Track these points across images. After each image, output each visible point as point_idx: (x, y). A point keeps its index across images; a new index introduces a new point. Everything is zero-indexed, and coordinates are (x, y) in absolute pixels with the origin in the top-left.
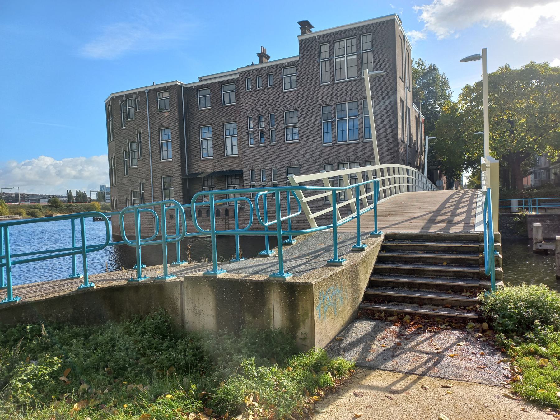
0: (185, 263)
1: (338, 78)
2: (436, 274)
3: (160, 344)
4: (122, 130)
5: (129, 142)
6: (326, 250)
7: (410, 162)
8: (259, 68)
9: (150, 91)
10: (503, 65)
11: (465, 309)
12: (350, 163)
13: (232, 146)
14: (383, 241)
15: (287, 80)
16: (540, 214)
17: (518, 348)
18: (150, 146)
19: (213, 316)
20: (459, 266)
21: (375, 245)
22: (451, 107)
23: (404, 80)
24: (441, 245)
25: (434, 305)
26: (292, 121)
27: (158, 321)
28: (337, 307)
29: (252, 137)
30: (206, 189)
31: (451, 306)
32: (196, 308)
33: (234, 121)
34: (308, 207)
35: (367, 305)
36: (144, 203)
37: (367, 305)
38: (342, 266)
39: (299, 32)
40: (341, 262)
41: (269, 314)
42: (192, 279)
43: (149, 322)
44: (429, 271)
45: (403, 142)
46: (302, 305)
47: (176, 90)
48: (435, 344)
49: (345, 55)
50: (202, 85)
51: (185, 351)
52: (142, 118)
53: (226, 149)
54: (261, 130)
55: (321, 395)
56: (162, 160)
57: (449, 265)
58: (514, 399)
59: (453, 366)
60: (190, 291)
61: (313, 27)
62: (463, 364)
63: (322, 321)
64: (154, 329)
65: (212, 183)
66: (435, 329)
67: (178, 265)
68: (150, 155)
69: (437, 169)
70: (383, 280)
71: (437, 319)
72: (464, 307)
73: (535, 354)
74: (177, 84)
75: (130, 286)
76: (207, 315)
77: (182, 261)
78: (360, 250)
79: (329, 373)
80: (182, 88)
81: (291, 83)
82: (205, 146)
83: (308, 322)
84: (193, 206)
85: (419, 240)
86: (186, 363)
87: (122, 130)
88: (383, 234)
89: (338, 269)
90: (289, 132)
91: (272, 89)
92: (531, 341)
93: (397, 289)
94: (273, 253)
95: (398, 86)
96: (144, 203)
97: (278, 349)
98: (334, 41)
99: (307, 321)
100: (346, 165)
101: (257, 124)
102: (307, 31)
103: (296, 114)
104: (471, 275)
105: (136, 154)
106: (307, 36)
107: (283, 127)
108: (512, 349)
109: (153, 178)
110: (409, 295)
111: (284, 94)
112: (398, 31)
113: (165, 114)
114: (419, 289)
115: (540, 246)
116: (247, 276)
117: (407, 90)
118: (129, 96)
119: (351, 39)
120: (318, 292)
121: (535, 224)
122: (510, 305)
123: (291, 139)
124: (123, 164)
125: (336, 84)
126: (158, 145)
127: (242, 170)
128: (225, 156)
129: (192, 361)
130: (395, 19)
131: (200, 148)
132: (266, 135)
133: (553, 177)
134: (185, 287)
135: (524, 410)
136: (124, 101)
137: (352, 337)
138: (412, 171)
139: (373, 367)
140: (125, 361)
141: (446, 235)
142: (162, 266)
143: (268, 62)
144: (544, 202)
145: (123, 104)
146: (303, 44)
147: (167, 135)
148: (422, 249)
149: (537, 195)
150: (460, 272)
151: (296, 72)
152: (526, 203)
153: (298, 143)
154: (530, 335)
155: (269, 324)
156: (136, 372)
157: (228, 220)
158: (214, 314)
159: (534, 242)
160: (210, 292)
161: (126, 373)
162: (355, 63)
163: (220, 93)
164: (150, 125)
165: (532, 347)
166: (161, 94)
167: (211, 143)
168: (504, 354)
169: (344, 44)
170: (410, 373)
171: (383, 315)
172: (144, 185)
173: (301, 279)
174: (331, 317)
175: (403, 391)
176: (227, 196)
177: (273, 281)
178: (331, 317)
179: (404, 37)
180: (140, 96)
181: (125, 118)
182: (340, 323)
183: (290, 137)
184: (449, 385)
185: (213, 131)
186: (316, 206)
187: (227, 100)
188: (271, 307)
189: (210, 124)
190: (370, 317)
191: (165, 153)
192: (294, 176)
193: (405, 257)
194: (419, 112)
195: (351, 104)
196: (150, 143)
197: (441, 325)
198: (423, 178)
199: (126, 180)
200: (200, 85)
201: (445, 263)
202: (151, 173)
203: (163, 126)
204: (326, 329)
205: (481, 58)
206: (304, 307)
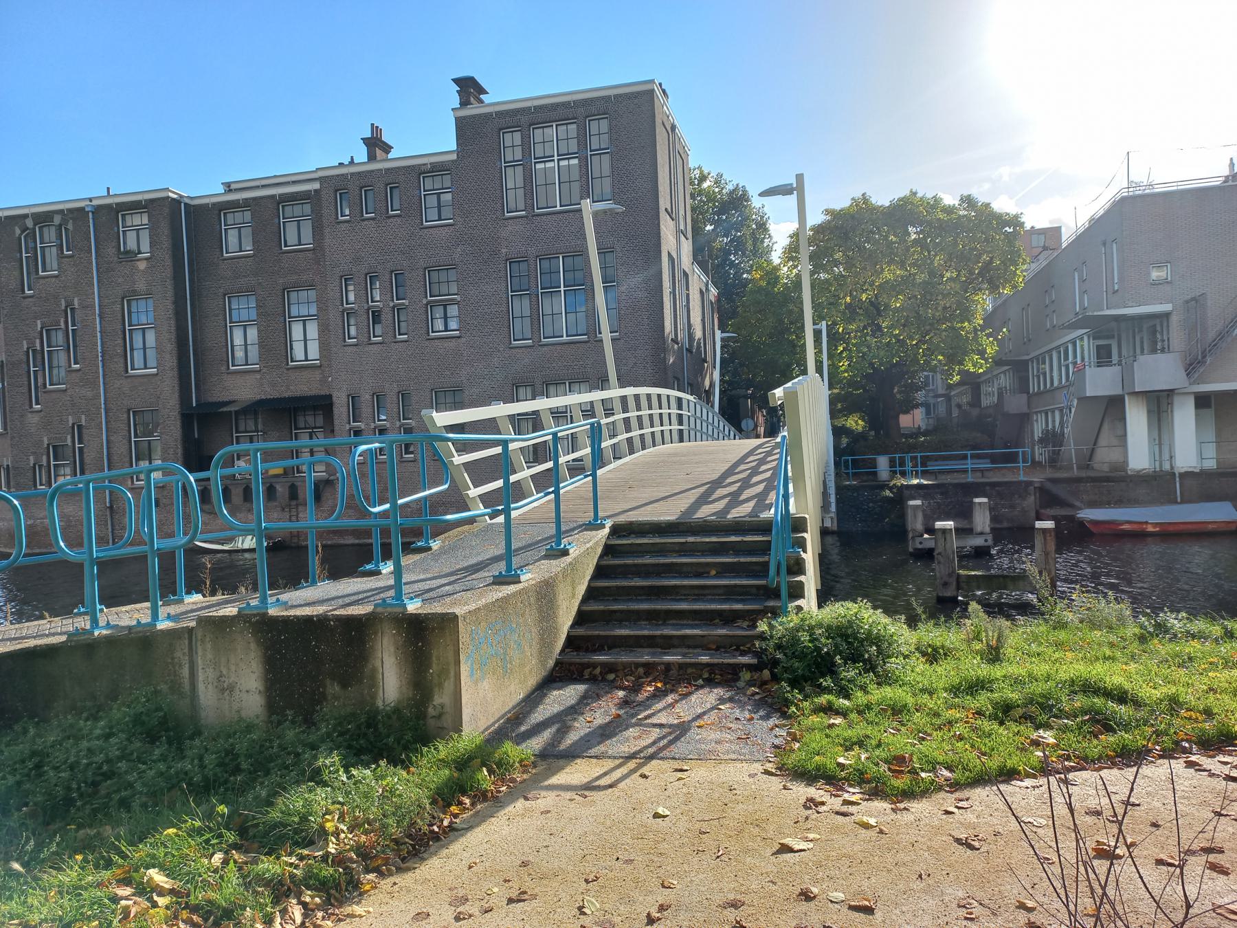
0: (197, 597)
1: (542, 203)
2: (696, 592)
3: (145, 753)
4: (24, 298)
5: (42, 328)
6: (496, 559)
7: (690, 382)
8: (368, 172)
9: (98, 210)
10: (858, 195)
11: (737, 649)
12: (569, 383)
13: (305, 340)
14: (608, 537)
15: (433, 201)
16: (926, 482)
17: (806, 704)
18: (99, 337)
19: (260, 692)
20: (734, 577)
21: (591, 544)
22: (767, 273)
23: (674, 216)
24: (707, 540)
25: (689, 647)
26: (444, 289)
27: (140, 709)
28: (508, 658)
29: (352, 321)
30: (242, 440)
31: (717, 647)
32: (223, 679)
33: (311, 286)
34: (466, 475)
35: (575, 658)
36: (82, 473)
37: (575, 658)
38: (520, 582)
39: (455, 101)
40: (519, 576)
41: (373, 677)
42: (214, 622)
43: (119, 712)
44: (684, 587)
45: (675, 341)
46: (439, 654)
47: (166, 210)
48: (677, 711)
49: (556, 158)
50: (233, 201)
51: (201, 758)
52: (78, 270)
53: (291, 349)
54: (373, 306)
55: (466, 804)
56: (130, 371)
57: (719, 575)
58: (777, 775)
59: (699, 741)
60: (209, 646)
61: (484, 92)
62: (715, 735)
63: (476, 683)
64: (131, 726)
65: (256, 424)
66: (685, 687)
67: (181, 601)
68: (100, 359)
69: (746, 397)
70: (602, 607)
71: (690, 670)
72: (738, 645)
73: (829, 710)
74: (168, 197)
75: (73, 644)
76: (247, 691)
77: (188, 593)
78: (560, 553)
79: (484, 769)
80: (183, 205)
81: (439, 207)
82: (238, 340)
83: (449, 686)
84: (216, 474)
85: (673, 532)
86: (206, 778)
87: (24, 298)
88: (609, 524)
89: (511, 589)
90: (439, 312)
91: (399, 220)
92: (827, 690)
93: (627, 623)
94: (387, 568)
95: (662, 227)
96: (82, 473)
97: (391, 739)
98: (530, 125)
99: (446, 684)
100: (562, 386)
101: (365, 294)
102: (472, 99)
103: (453, 275)
104: (754, 591)
105: (62, 356)
106: (473, 110)
107: (425, 301)
108: (796, 705)
109: (106, 413)
110: (646, 632)
111: (426, 231)
112: (661, 116)
113: (138, 263)
114: (665, 621)
115: (921, 543)
116: (335, 610)
117: (682, 235)
118: (43, 219)
119: (567, 124)
120: (469, 629)
121: (912, 503)
122: (804, 637)
123: (442, 328)
124: (26, 379)
125: (538, 215)
126: (121, 336)
127: (330, 396)
128: (288, 364)
129: (215, 775)
130: (654, 90)
131: (226, 346)
132: (386, 317)
133: (955, 413)
134: (199, 638)
135: (785, 788)
136: (28, 228)
137: (540, 714)
138: (688, 401)
139: (571, 755)
140: (69, 789)
141: (719, 522)
142: (148, 604)
143: (388, 160)
144: (936, 461)
145: (25, 237)
146: (463, 126)
147: (144, 312)
148: (677, 549)
149: (922, 447)
150: (736, 586)
151: (450, 185)
152: (902, 464)
153: (459, 337)
154: (827, 682)
155: (374, 697)
156: (94, 806)
157: (297, 508)
158: (261, 688)
159: (910, 535)
160: (253, 646)
161: (73, 810)
162: (575, 175)
163: (277, 220)
164: (99, 288)
165: (823, 699)
166: (128, 218)
167: (253, 333)
168: (784, 715)
169: (551, 132)
170: (632, 756)
171: (598, 670)
172: (84, 431)
173: (437, 608)
174: (496, 677)
175: (611, 786)
176: (297, 453)
177: (383, 613)
178: (496, 677)
179: (673, 127)
180: (71, 218)
181: (32, 269)
182: (516, 691)
183: (439, 325)
184: (685, 768)
185: (258, 307)
186: (481, 472)
187: (291, 236)
188: (378, 664)
189: (249, 291)
190: (575, 676)
191: (138, 356)
192: (434, 414)
193: (645, 565)
194: (708, 282)
195: (569, 261)
196: (98, 329)
197: (696, 681)
198: (712, 415)
199: (33, 419)
200: (228, 202)
201: (713, 572)
202: (103, 402)
203: (134, 293)
204: (484, 698)
205: (795, 192)
206: (441, 658)
